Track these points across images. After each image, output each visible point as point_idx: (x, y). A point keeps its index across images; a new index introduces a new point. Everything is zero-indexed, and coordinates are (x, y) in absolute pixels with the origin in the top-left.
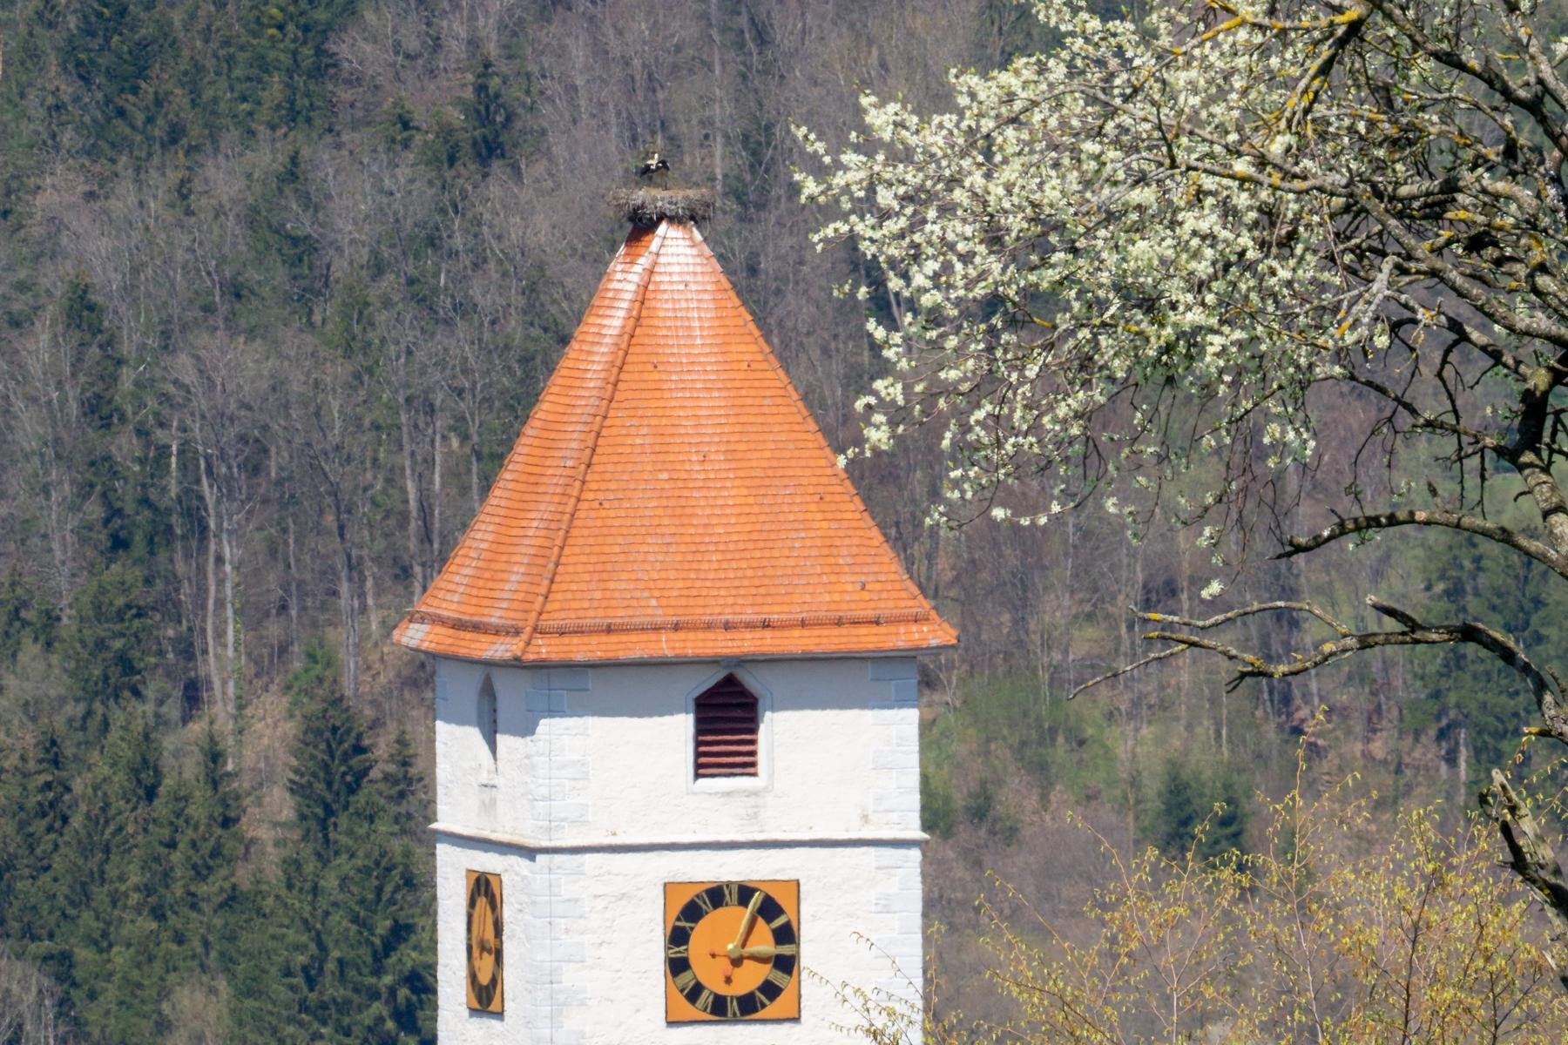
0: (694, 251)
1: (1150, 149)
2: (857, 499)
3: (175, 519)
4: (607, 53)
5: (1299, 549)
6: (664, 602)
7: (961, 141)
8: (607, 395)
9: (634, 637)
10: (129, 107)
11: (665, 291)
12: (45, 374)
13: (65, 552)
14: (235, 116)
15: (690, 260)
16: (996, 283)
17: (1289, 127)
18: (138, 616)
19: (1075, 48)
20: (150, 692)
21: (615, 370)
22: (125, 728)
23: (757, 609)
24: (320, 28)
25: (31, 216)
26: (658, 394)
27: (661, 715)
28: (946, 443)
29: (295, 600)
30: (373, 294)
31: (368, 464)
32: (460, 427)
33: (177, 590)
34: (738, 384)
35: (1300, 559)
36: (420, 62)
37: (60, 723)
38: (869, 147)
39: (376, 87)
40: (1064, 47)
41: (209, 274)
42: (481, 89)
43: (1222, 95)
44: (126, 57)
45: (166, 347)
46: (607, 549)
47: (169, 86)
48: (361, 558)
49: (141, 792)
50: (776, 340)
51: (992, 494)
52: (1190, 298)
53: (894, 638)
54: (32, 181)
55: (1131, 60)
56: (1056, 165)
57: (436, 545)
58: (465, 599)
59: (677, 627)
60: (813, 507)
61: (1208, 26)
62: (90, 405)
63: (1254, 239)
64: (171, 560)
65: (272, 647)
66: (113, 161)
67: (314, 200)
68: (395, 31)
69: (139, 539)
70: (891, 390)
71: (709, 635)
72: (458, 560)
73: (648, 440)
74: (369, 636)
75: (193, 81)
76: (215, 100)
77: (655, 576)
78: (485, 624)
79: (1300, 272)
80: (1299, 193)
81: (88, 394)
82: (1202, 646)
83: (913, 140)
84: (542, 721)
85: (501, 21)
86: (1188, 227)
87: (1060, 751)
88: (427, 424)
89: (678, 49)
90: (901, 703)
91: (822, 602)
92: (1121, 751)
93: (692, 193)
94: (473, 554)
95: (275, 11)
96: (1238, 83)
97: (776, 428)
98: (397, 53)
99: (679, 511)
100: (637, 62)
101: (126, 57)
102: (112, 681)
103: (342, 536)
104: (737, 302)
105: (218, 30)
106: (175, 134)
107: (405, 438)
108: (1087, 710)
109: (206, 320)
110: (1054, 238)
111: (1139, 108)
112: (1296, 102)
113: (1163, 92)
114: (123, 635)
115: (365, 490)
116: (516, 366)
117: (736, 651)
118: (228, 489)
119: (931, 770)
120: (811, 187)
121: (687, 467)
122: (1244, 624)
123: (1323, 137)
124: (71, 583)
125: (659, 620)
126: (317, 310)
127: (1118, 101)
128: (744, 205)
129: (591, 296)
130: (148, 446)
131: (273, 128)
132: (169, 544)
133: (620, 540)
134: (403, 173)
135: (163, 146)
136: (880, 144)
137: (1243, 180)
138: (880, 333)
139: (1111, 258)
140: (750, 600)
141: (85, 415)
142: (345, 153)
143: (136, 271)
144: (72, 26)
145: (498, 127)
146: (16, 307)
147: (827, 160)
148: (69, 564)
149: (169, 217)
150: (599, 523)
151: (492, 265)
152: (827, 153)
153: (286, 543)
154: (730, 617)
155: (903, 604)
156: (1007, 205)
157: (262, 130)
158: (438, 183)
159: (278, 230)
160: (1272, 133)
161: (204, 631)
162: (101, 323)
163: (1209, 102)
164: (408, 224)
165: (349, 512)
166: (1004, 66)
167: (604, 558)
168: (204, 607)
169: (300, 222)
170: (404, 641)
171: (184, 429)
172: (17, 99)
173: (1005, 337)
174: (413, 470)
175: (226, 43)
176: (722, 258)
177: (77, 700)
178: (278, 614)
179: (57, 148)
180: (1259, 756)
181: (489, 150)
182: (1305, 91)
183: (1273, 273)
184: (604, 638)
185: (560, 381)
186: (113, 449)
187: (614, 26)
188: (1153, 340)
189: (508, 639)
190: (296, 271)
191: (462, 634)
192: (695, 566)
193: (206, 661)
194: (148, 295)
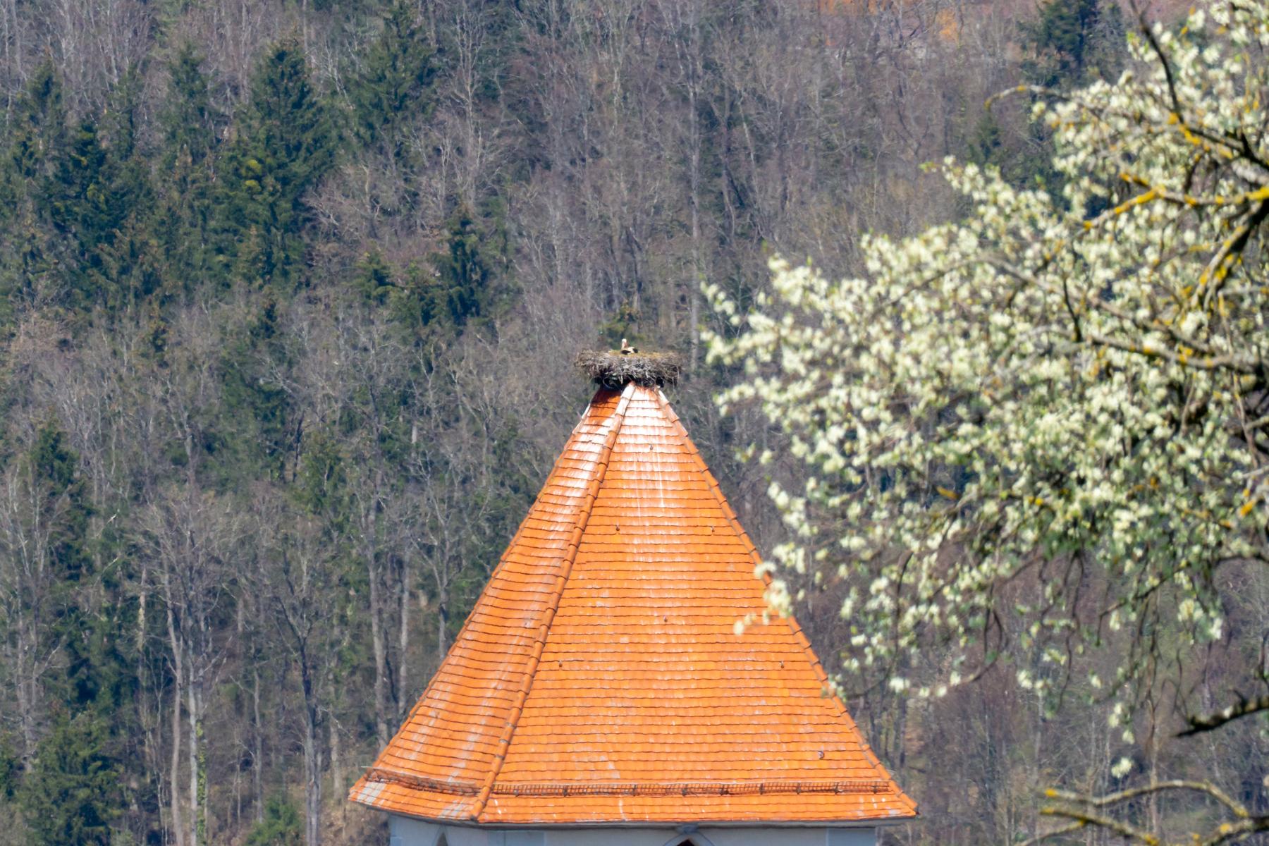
0: (660, 414)
3: (140, 671)
5: (1200, 727)
6: (621, 765)
8: (569, 557)
9: (590, 801)
10: (105, 257)
13: (29, 701)
14: (209, 269)
15: (657, 423)
16: (902, 454)
18: (103, 768)
19: (987, 219)
21: (577, 531)
23: (716, 775)
24: (298, 182)
30: (345, 451)
31: (335, 622)
32: (428, 585)
33: (142, 743)
35: (1203, 736)
36: (398, 218)
41: (181, 425)
42: (457, 246)
44: (104, 207)
46: (565, 712)
47: (145, 236)
48: (325, 714)
52: (1097, 473)
56: (966, 335)
57: (401, 704)
58: (422, 757)
59: (635, 792)
60: (774, 675)
62: (59, 554)
64: (136, 711)
66: (87, 310)
67: (289, 355)
68: (374, 187)
70: (792, 556)
71: (667, 800)
73: (609, 603)
74: (332, 794)
75: (169, 229)
76: (190, 251)
79: (1209, 450)
80: (1208, 369)
81: (58, 543)
83: (822, 305)
85: (478, 178)
88: (395, 581)
89: (658, 209)
91: (781, 770)
93: (659, 356)
94: (432, 713)
95: (253, 163)
96: (1152, 256)
97: (739, 595)
99: (639, 675)
100: (615, 223)
101: (104, 207)
103: (308, 691)
104: (703, 466)
105: (194, 182)
106: (150, 283)
107: (373, 595)
109: (176, 471)
110: (961, 410)
111: (1049, 280)
112: (1207, 278)
114: (87, 786)
115: (332, 645)
116: (485, 525)
118: (194, 640)
120: (718, 347)
123: (1236, 314)
124: (34, 732)
125: (615, 784)
126: (289, 466)
130: (116, 596)
131: (250, 280)
133: (578, 703)
134: (379, 329)
135: (136, 296)
136: (787, 307)
137: (1152, 357)
138: (781, 499)
141: (53, 564)
144: (50, 174)
145: (474, 285)
148: (34, 714)
149: (142, 366)
150: (558, 685)
154: (689, 783)
156: (914, 373)
157: (239, 284)
158: (412, 340)
159: (252, 384)
160: (1183, 310)
162: (71, 473)
164: (381, 381)
165: (314, 667)
167: (562, 721)
168: (168, 759)
169: (271, 375)
170: (360, 798)
171: (152, 581)
173: (908, 506)
174: (380, 627)
175: (202, 195)
178: (243, 769)
179: (33, 295)
182: (1218, 268)
183: (1182, 451)
184: (562, 801)
186: (80, 599)
188: (1059, 514)
189: (464, 800)
190: (267, 426)
191: (418, 793)
192: (655, 730)
193: (170, 814)
194: (119, 445)
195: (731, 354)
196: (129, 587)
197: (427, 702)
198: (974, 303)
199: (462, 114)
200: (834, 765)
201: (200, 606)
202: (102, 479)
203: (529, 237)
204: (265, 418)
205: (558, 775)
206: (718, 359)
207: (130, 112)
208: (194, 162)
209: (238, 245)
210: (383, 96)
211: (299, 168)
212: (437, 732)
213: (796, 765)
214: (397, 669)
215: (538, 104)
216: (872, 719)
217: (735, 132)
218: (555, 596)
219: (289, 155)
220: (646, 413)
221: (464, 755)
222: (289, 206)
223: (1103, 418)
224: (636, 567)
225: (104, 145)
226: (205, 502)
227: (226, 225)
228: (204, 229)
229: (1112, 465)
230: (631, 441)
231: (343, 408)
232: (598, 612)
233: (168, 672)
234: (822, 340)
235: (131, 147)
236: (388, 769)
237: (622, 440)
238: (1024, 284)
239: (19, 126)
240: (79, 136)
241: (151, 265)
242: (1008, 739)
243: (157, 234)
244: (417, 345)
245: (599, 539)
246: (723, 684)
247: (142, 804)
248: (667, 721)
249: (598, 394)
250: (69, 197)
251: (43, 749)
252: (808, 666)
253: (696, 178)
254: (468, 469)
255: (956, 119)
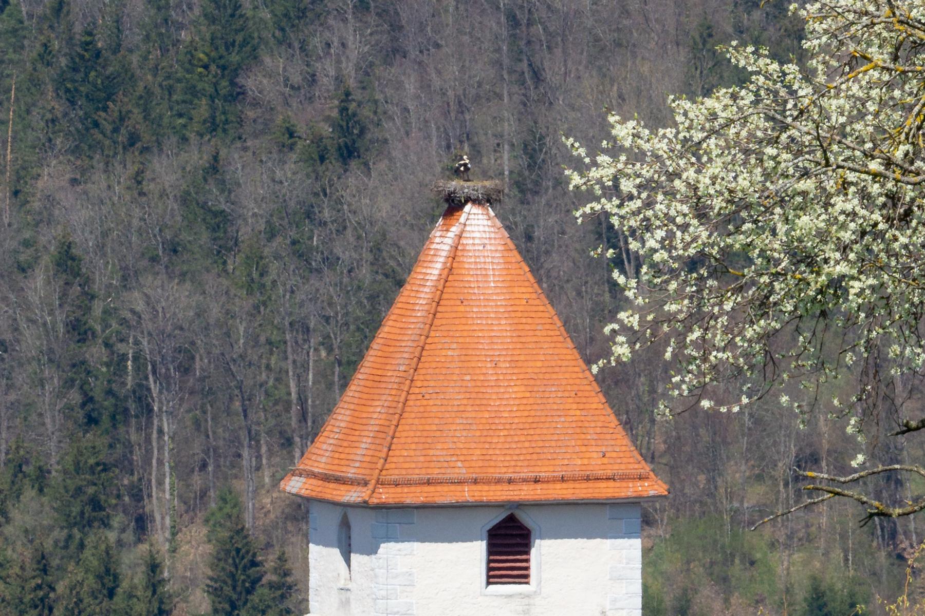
0: (489, 223)
1: (809, 153)
2: (600, 395)
4: (429, 86)
6: (467, 464)
7: (679, 147)
8: (429, 322)
9: (446, 488)
11: (469, 251)
12: (41, 304)
14: (174, 128)
15: (487, 229)
16: (704, 244)
17: (907, 138)
18: (104, 470)
20: (116, 522)
21: (434, 304)
22: (96, 548)
23: (531, 469)
24: (233, 68)
25: (33, 195)
26: (464, 321)
27: (450, 541)
28: (668, 355)
29: (212, 461)
33: (131, 452)
34: (520, 315)
37: (48, 544)
38: (615, 151)
39: (272, 109)
40: (752, 83)
41: (155, 236)
42: (343, 110)
43: (862, 116)
45: (125, 286)
46: (427, 428)
47: (130, 107)
49: (105, 592)
50: (545, 285)
51: (700, 391)
52: (838, 255)
53: (625, 490)
54: (35, 171)
55: (796, 91)
56: (745, 163)
57: (310, 424)
58: (330, 460)
59: (475, 482)
61: (851, 69)
63: (882, 215)
64: (127, 432)
65: (196, 493)
69: (105, 419)
70: (631, 319)
71: (499, 487)
72: (325, 434)
73: (456, 353)
74: (263, 486)
76: (161, 117)
77: (461, 446)
78: (343, 478)
79: (915, 238)
80: (914, 184)
82: (843, 495)
84: (382, 545)
86: (838, 208)
87: (737, 569)
88: (304, 341)
90: (629, 535)
91: (577, 465)
92: (780, 570)
93: (488, 184)
95: (201, 56)
96: (872, 107)
98: (286, 86)
100: (450, 93)
102: (87, 515)
104: (519, 258)
105: (163, 69)
106: (133, 139)
107: (289, 349)
108: (756, 541)
110: (744, 214)
113: (820, 113)
114: (95, 484)
115: (261, 385)
117: (517, 498)
118: (166, 382)
119: (650, 581)
120: (576, 180)
121: (484, 371)
122: (865, 483)
125: (462, 477)
127: (789, 120)
128: (522, 191)
129: (418, 254)
132: (126, 423)
134: (290, 166)
135: (124, 148)
136: (622, 149)
137: (875, 175)
138: (621, 280)
139: (781, 228)
140: (526, 463)
141: (68, 332)
142: (250, 153)
143: (105, 234)
145: (355, 137)
146: (22, 258)
147: (587, 160)
148: (57, 434)
151: (349, 232)
152: (587, 156)
153: (206, 421)
155: (631, 466)
156: (712, 192)
157: (192, 136)
158: (313, 175)
159: (204, 206)
161: (150, 481)
162: (80, 269)
163: (851, 120)
164: (292, 204)
165: (250, 400)
166: (707, 93)
167: (425, 434)
168: (150, 464)
169: (217, 200)
170: (288, 489)
171: (137, 343)
172: (24, 115)
173: (710, 282)
176: (508, 228)
177: (62, 528)
178: (200, 470)
180: (875, 574)
181: (348, 153)
182: (918, 114)
183: (896, 239)
185: (396, 311)
187: (436, 68)
188: (812, 284)
191: (327, 484)
197: (332, 422)
199: (345, 20)
200: (612, 461)
201: (170, 359)
202: (103, 275)
203: (392, 103)
204: (214, 230)
207: (117, 22)
208: (162, 55)
209: (193, 112)
210: (291, 9)
211: (234, 58)
212: (340, 443)
214: (306, 400)
215: (397, 13)
216: (632, 430)
217: (533, 30)
219: (227, 49)
220: (480, 222)
222: (227, 83)
225: (100, 45)
226: (172, 288)
228: (169, 100)
229: (848, 251)
230: (471, 242)
231: (267, 222)
232: (449, 359)
233: (148, 405)
235: (119, 45)
236: (308, 467)
237: (464, 241)
239: (41, 33)
240: (83, 39)
241: (134, 127)
242: (725, 442)
244: (317, 178)
247: (132, 496)
248: (497, 433)
250: (77, 81)
251: (62, 459)
252: (593, 394)
253: (506, 61)
255: (683, 19)
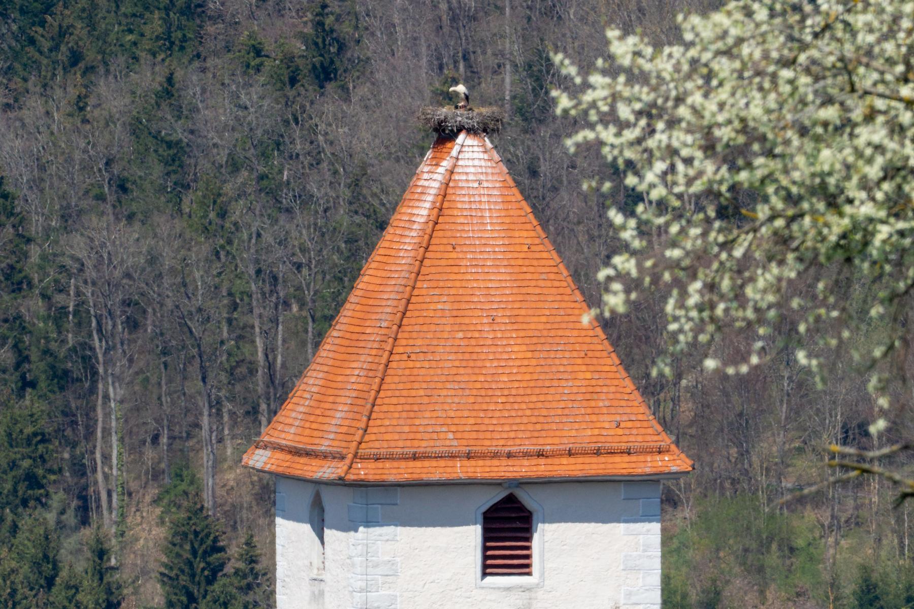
14: (122, 45)
15: (483, 163)
23: (534, 441)
47: (71, 21)
52: (863, 195)
56: (761, 89)
58: (300, 431)
59: (469, 456)
71: (495, 462)
83: (647, 66)
91: (585, 437)
94: (307, 396)
104: (519, 197)
106: (76, 58)
125: (454, 449)
133: (424, 386)
135: (64, 69)
136: (620, 70)
158: (283, 101)
162: (13, 208)
164: (259, 132)
167: (410, 400)
170: (251, 463)
181: (325, 74)
184: (411, 464)
189: (334, 464)
192: (484, 407)
195: (575, 107)
196: (59, 298)
198: (768, 65)
203: (375, 17)
205: (408, 443)
206: (566, 111)
213: (596, 432)
218: (404, 302)
220: (476, 155)
221: (334, 429)
223: (868, 151)
224: (469, 277)
227: (135, 10)
231: (229, 154)
232: (439, 314)
234: (648, 94)
236: (272, 439)
238: (804, 47)
243: (80, 18)
245: (439, 255)
246: (539, 369)
248: (494, 399)
249: (438, 139)
254: (328, 202)
